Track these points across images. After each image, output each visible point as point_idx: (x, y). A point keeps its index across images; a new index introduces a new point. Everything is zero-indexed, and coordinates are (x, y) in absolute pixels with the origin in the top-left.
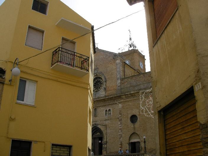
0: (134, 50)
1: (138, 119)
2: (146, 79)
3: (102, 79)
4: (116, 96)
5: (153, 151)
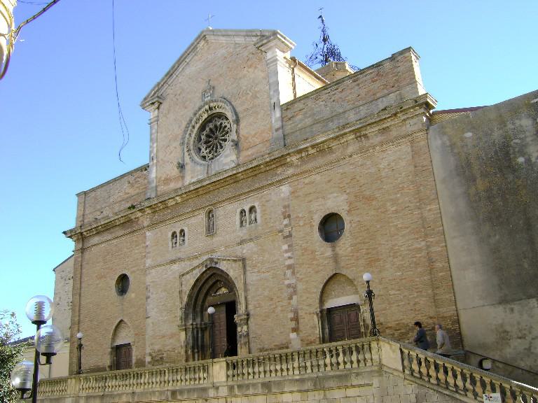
1: (347, 226)
2: (363, 92)
3: (227, 119)
4: (268, 160)
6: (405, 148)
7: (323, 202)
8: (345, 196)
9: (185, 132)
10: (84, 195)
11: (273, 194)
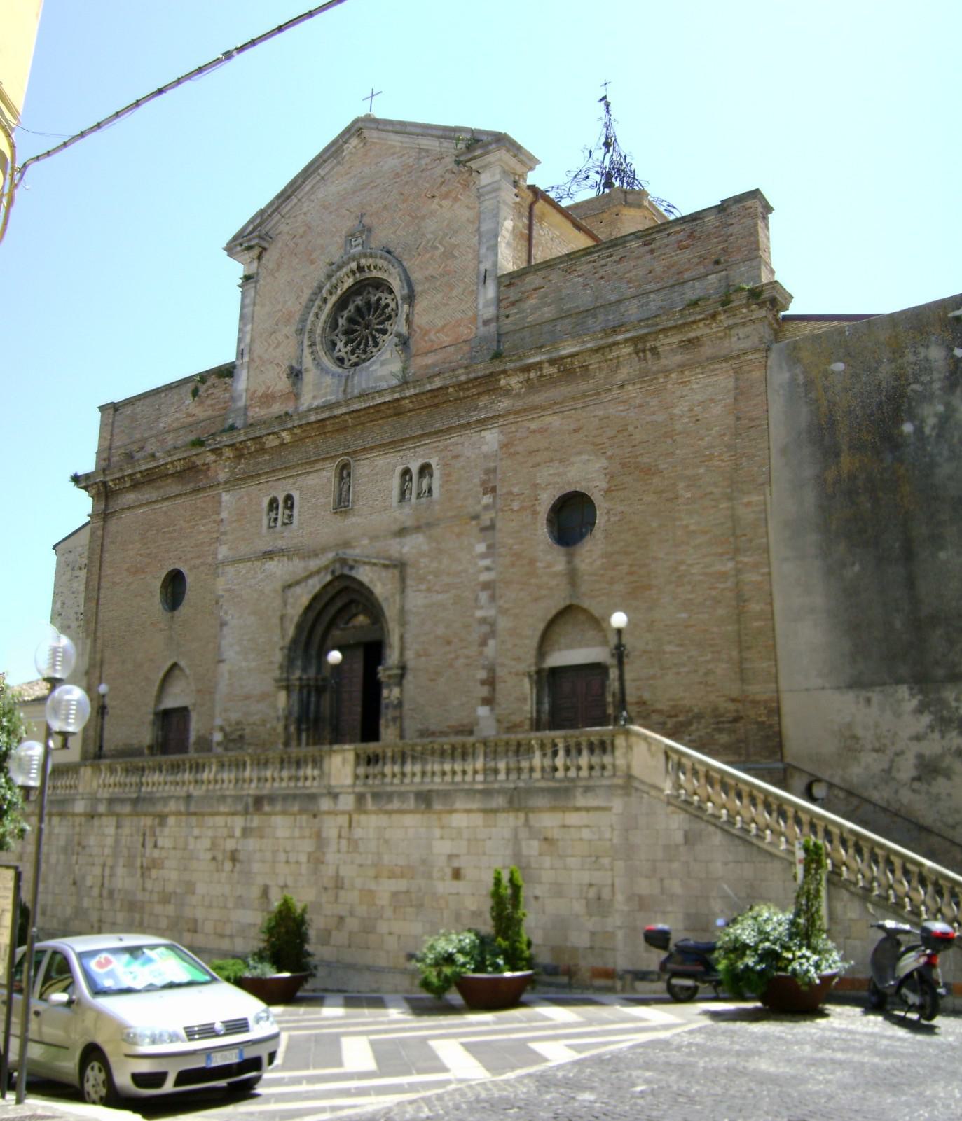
0: (626, 192)
1: (601, 520)
2: (658, 268)
3: (391, 292)
4: (463, 378)
5: (690, 723)
6: (723, 380)
7: (561, 470)
8: (603, 462)
9: (308, 308)
10: (111, 410)
11: (466, 444)
